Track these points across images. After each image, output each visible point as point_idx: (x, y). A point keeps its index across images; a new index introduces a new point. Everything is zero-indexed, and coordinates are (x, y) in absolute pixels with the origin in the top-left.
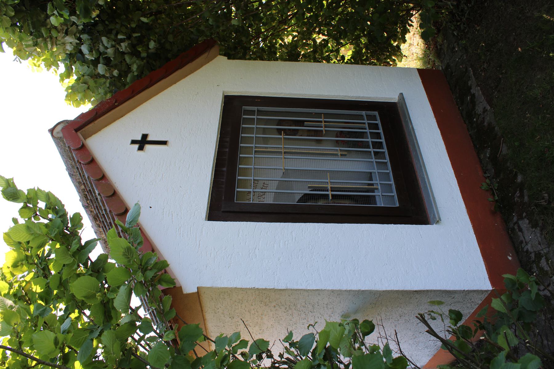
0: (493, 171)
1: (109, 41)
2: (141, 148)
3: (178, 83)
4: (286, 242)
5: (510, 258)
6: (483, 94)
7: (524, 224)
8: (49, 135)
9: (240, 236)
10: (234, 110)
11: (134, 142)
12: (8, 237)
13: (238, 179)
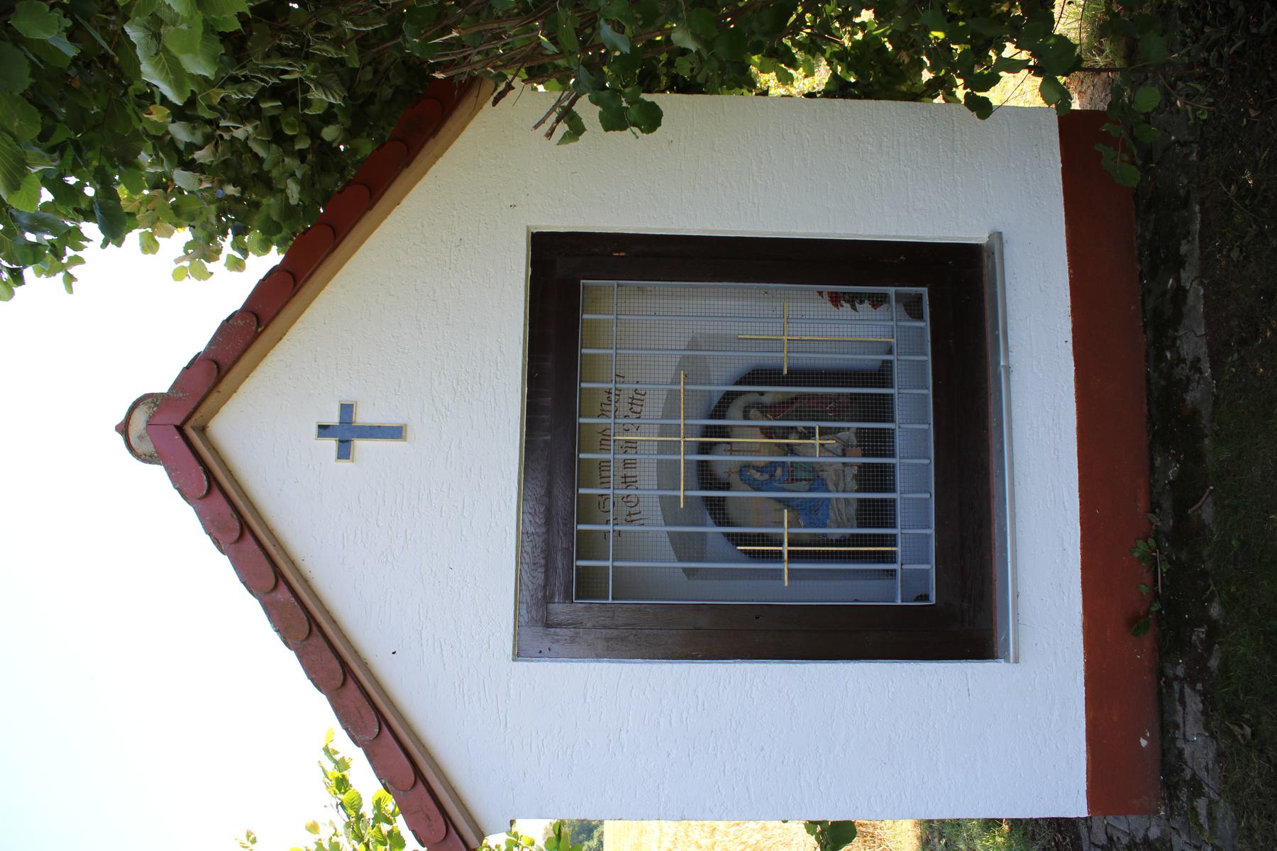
0: (1171, 522)
1: (194, 128)
2: (344, 452)
3: (405, 202)
4: (685, 714)
5: (1144, 743)
6: (1207, 315)
7: (1194, 704)
8: (120, 439)
9: (588, 700)
10: (566, 273)
11: (324, 430)
12: (119, 245)
13: (578, 532)
